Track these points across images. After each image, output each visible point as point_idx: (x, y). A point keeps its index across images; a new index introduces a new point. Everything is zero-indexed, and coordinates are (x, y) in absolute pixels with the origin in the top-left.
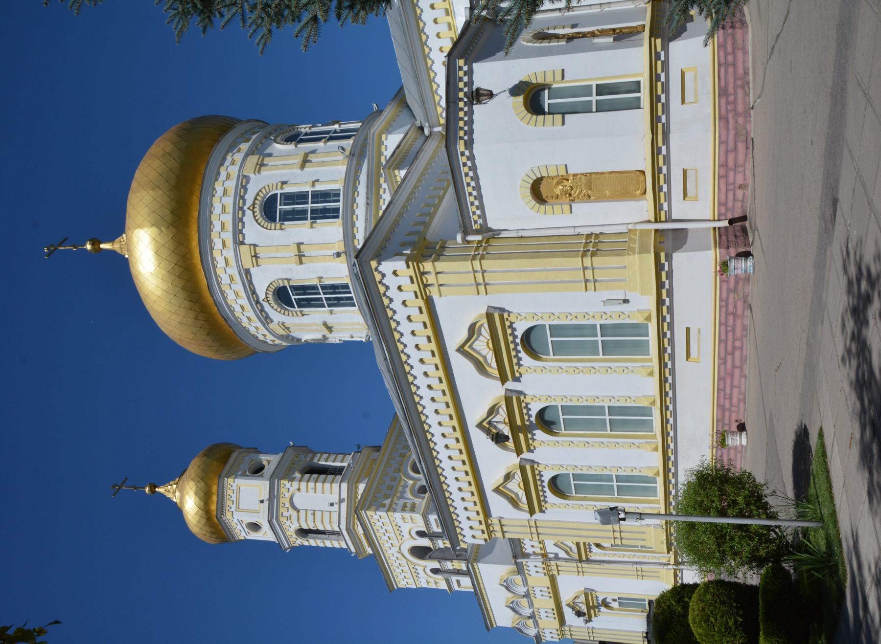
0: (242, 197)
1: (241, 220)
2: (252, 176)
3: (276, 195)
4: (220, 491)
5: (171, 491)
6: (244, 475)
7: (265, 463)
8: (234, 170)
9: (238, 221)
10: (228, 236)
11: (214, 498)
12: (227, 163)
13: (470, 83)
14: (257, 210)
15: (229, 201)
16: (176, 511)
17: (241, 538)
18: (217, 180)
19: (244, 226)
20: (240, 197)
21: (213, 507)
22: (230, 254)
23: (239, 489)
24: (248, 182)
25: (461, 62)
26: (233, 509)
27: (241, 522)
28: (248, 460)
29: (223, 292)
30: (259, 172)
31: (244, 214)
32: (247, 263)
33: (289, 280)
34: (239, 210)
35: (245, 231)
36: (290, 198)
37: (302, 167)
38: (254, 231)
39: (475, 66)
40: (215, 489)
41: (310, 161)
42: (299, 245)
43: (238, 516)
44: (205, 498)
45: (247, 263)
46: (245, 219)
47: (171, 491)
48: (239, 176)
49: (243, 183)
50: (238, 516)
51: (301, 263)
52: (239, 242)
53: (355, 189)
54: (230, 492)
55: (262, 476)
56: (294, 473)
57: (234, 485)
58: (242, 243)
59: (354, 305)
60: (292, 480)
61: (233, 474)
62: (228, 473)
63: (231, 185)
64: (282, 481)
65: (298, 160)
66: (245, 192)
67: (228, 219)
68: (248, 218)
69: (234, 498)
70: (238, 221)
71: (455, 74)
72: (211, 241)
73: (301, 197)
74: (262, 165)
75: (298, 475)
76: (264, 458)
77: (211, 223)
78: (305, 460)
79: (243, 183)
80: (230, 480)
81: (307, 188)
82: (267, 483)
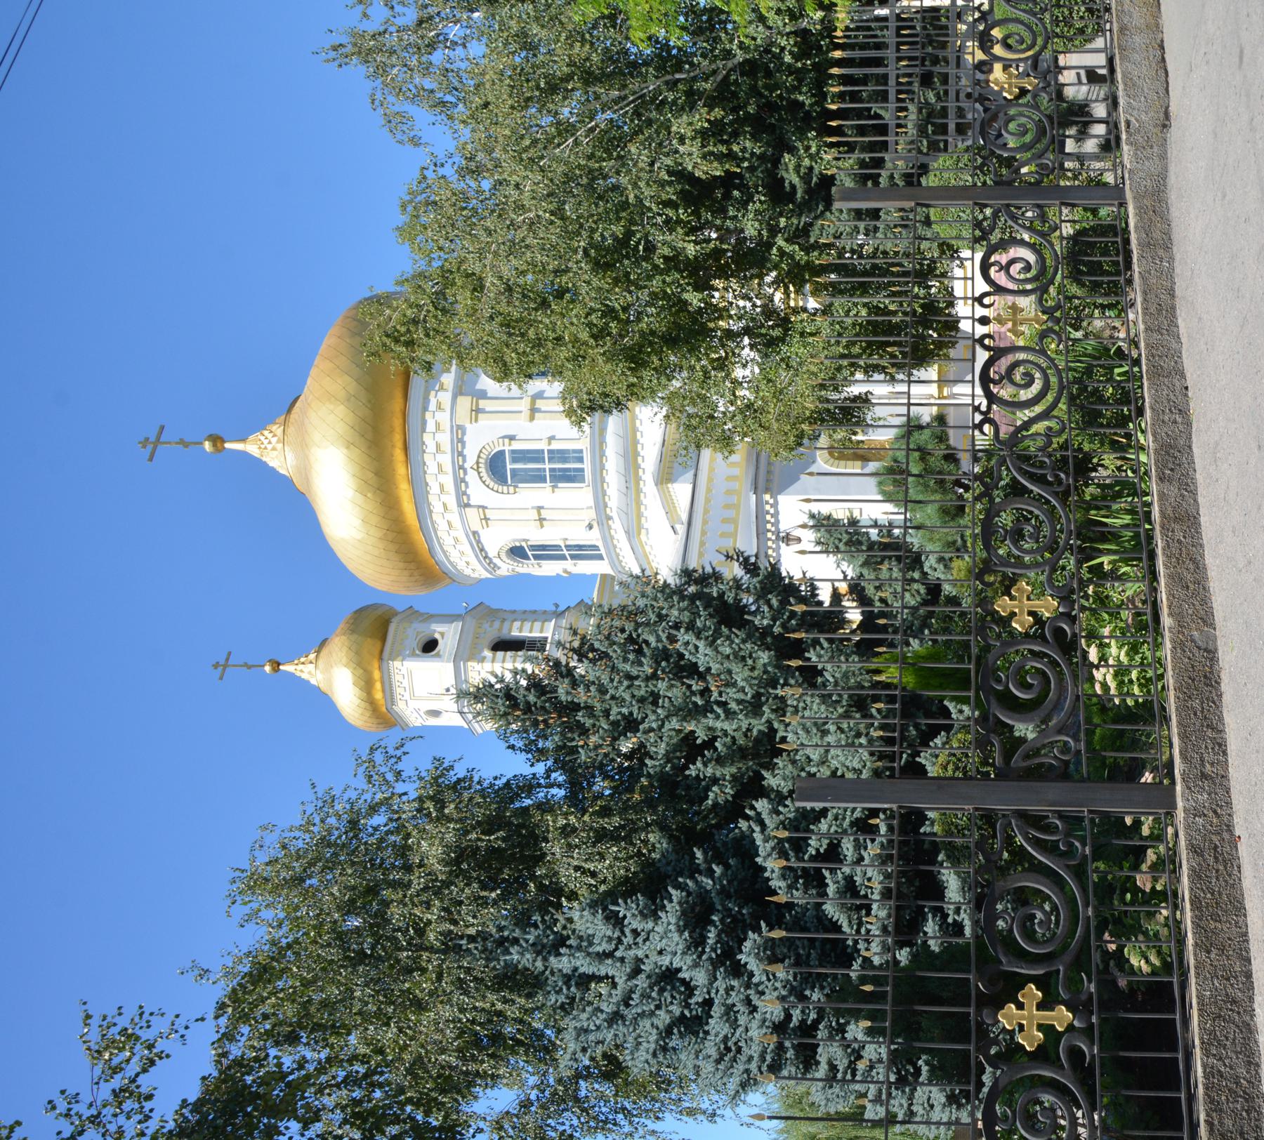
0: (461, 454)
1: (463, 480)
2: (468, 426)
3: (502, 453)
4: (386, 676)
5: (306, 670)
6: (413, 655)
7: (437, 636)
8: (444, 418)
9: (460, 482)
10: (451, 500)
11: (378, 686)
12: (432, 406)
13: (776, 524)
14: (482, 470)
15: (446, 460)
16: (321, 700)
17: (418, 724)
18: (424, 430)
19: (467, 486)
20: (459, 454)
21: (378, 695)
22: (454, 517)
23: (410, 673)
24: (464, 433)
25: (767, 497)
26: (407, 696)
27: (417, 711)
28: (415, 633)
29: (444, 552)
30: (476, 421)
31: (465, 473)
32: (475, 524)
33: (526, 541)
34: (459, 468)
35: (465, 452)
36: (519, 456)
37: (532, 418)
38: (479, 491)
39: (780, 498)
40: (377, 675)
41: (539, 411)
42: (539, 508)
43: (412, 704)
44: (366, 685)
45: (475, 524)
46: (467, 479)
47: (306, 670)
48: (452, 427)
49: (459, 436)
50: (412, 704)
51: (542, 526)
52: (464, 506)
53: (602, 454)
54: (398, 678)
55: (438, 655)
56: (482, 651)
57: (404, 671)
58: (468, 505)
59: (600, 557)
60: (482, 660)
61: (398, 654)
62: (390, 654)
63: (445, 438)
64: (469, 664)
65: (524, 405)
66: (463, 447)
67: (448, 481)
68: (472, 477)
69: (405, 683)
70: (460, 482)
71: (763, 507)
72: (429, 504)
73: (536, 456)
74: (478, 411)
75: (488, 653)
76: (437, 630)
77: (427, 484)
78: (493, 631)
79: (459, 436)
80: (397, 664)
81: (543, 446)
82: (451, 665)
